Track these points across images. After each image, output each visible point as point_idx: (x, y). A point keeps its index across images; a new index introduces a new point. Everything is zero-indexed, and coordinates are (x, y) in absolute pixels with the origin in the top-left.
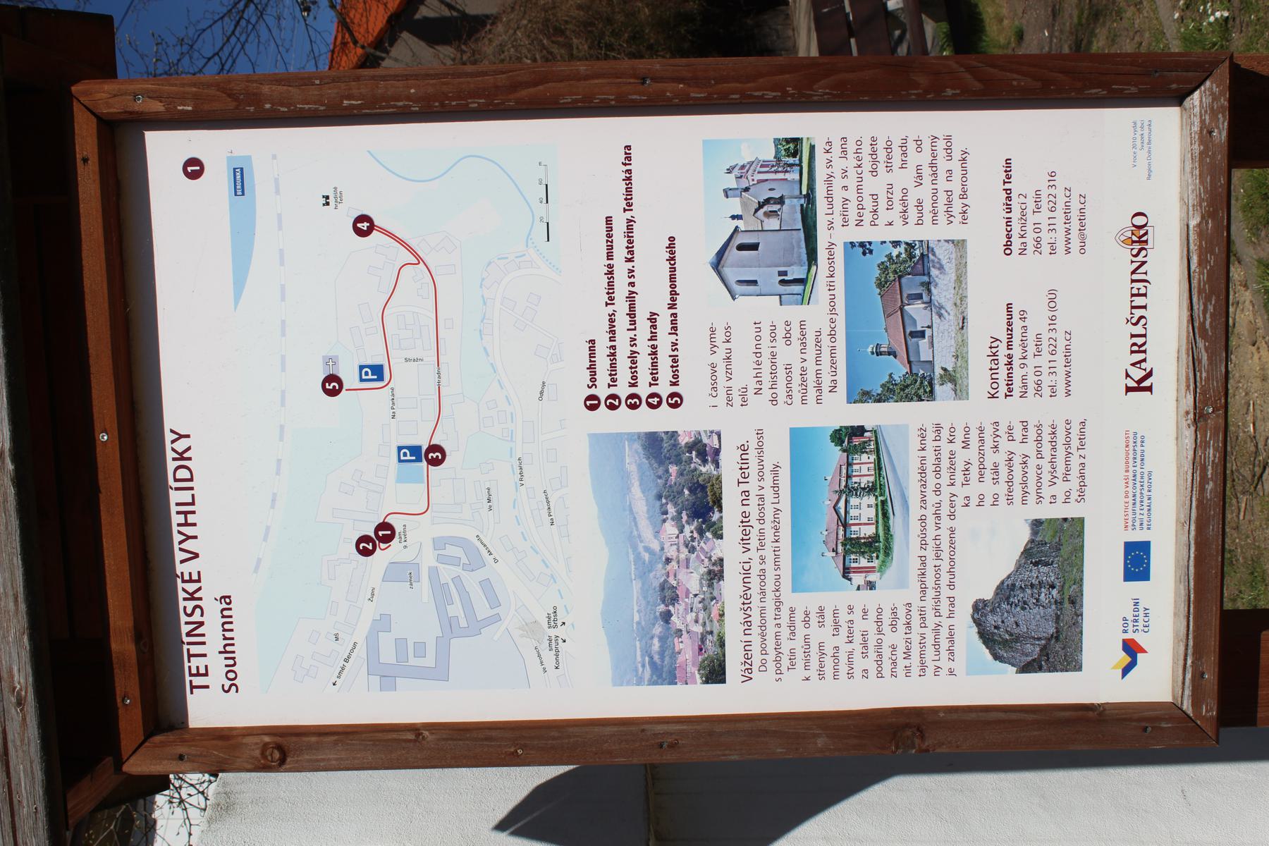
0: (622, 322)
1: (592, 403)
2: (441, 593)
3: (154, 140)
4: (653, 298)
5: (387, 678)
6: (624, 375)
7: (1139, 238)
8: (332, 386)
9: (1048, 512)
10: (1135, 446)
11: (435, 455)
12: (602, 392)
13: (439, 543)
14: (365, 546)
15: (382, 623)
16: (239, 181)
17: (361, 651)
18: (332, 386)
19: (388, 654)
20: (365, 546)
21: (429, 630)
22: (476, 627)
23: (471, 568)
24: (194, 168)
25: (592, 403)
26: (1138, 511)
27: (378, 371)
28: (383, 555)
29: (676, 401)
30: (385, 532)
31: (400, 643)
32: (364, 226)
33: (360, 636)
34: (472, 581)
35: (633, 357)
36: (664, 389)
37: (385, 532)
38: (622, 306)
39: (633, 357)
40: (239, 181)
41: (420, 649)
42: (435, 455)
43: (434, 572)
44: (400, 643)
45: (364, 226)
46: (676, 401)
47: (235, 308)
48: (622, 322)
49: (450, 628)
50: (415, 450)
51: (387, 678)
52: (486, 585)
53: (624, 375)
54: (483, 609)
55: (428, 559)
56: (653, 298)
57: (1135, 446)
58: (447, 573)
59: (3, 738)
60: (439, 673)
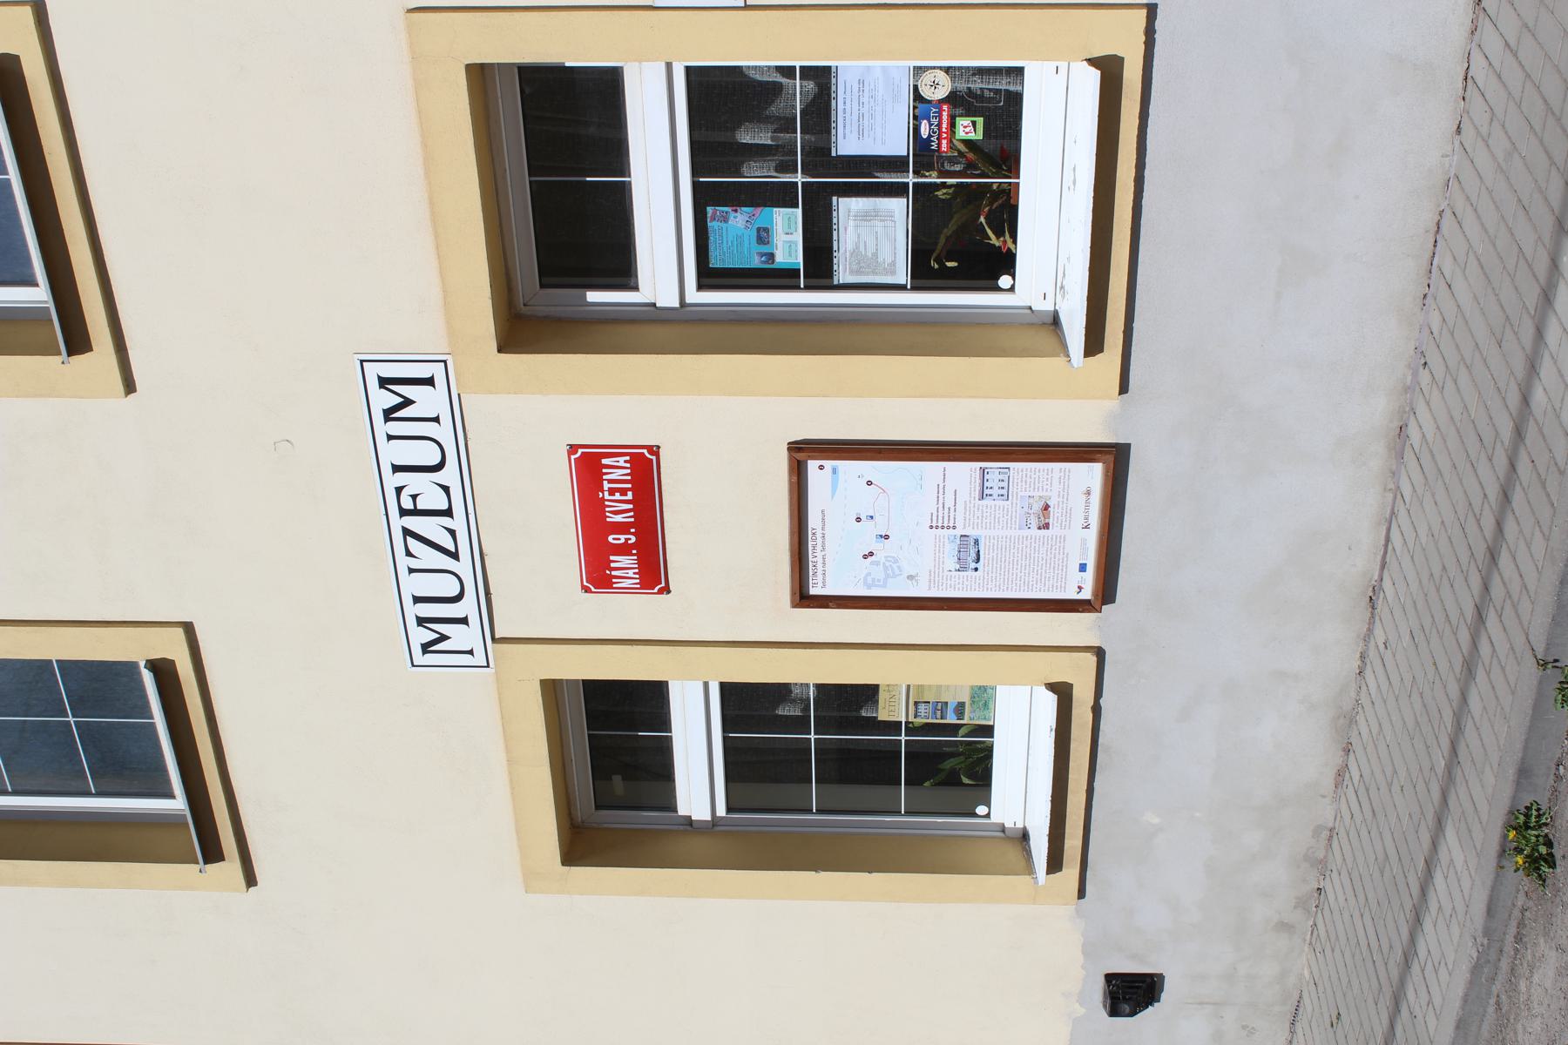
0: (941, 509)
1: (931, 527)
2: (886, 568)
3: (631, 498)
4: (949, 503)
5: (869, 587)
6: (940, 521)
7: (1088, 493)
8: (858, 520)
9: (1081, 562)
10: (1084, 541)
11: (887, 537)
12: (934, 525)
13: (886, 557)
14: (865, 557)
15: (869, 574)
16: (834, 471)
17: (862, 579)
18: (858, 520)
19: (869, 580)
20: (865, 557)
21: (881, 576)
22: (895, 576)
23: (894, 563)
24: (821, 468)
25: (931, 527)
26: (1004, 542)
27: (872, 517)
28: (870, 559)
29: (954, 528)
30: (871, 554)
31: (873, 580)
32: (869, 483)
33: (863, 576)
34: (895, 566)
35: (943, 517)
36: (951, 525)
37: (871, 554)
38: (940, 505)
39: (943, 517)
40: (834, 471)
41: (879, 581)
42: (887, 537)
43: (884, 563)
44: (873, 580)
45: (869, 483)
46: (954, 528)
47: (832, 498)
48: (941, 509)
49: (887, 576)
50: (881, 536)
51: (869, 587)
52: (899, 567)
53: (940, 521)
54: (897, 572)
55: (883, 560)
56: (949, 503)
57: (1084, 541)
58: (887, 564)
59: (607, 319)
60: (884, 586)
